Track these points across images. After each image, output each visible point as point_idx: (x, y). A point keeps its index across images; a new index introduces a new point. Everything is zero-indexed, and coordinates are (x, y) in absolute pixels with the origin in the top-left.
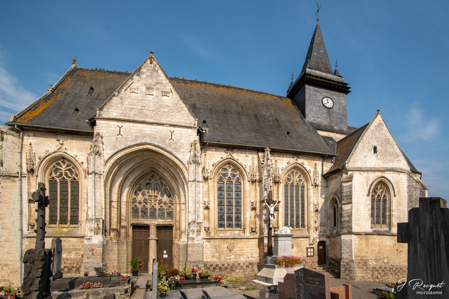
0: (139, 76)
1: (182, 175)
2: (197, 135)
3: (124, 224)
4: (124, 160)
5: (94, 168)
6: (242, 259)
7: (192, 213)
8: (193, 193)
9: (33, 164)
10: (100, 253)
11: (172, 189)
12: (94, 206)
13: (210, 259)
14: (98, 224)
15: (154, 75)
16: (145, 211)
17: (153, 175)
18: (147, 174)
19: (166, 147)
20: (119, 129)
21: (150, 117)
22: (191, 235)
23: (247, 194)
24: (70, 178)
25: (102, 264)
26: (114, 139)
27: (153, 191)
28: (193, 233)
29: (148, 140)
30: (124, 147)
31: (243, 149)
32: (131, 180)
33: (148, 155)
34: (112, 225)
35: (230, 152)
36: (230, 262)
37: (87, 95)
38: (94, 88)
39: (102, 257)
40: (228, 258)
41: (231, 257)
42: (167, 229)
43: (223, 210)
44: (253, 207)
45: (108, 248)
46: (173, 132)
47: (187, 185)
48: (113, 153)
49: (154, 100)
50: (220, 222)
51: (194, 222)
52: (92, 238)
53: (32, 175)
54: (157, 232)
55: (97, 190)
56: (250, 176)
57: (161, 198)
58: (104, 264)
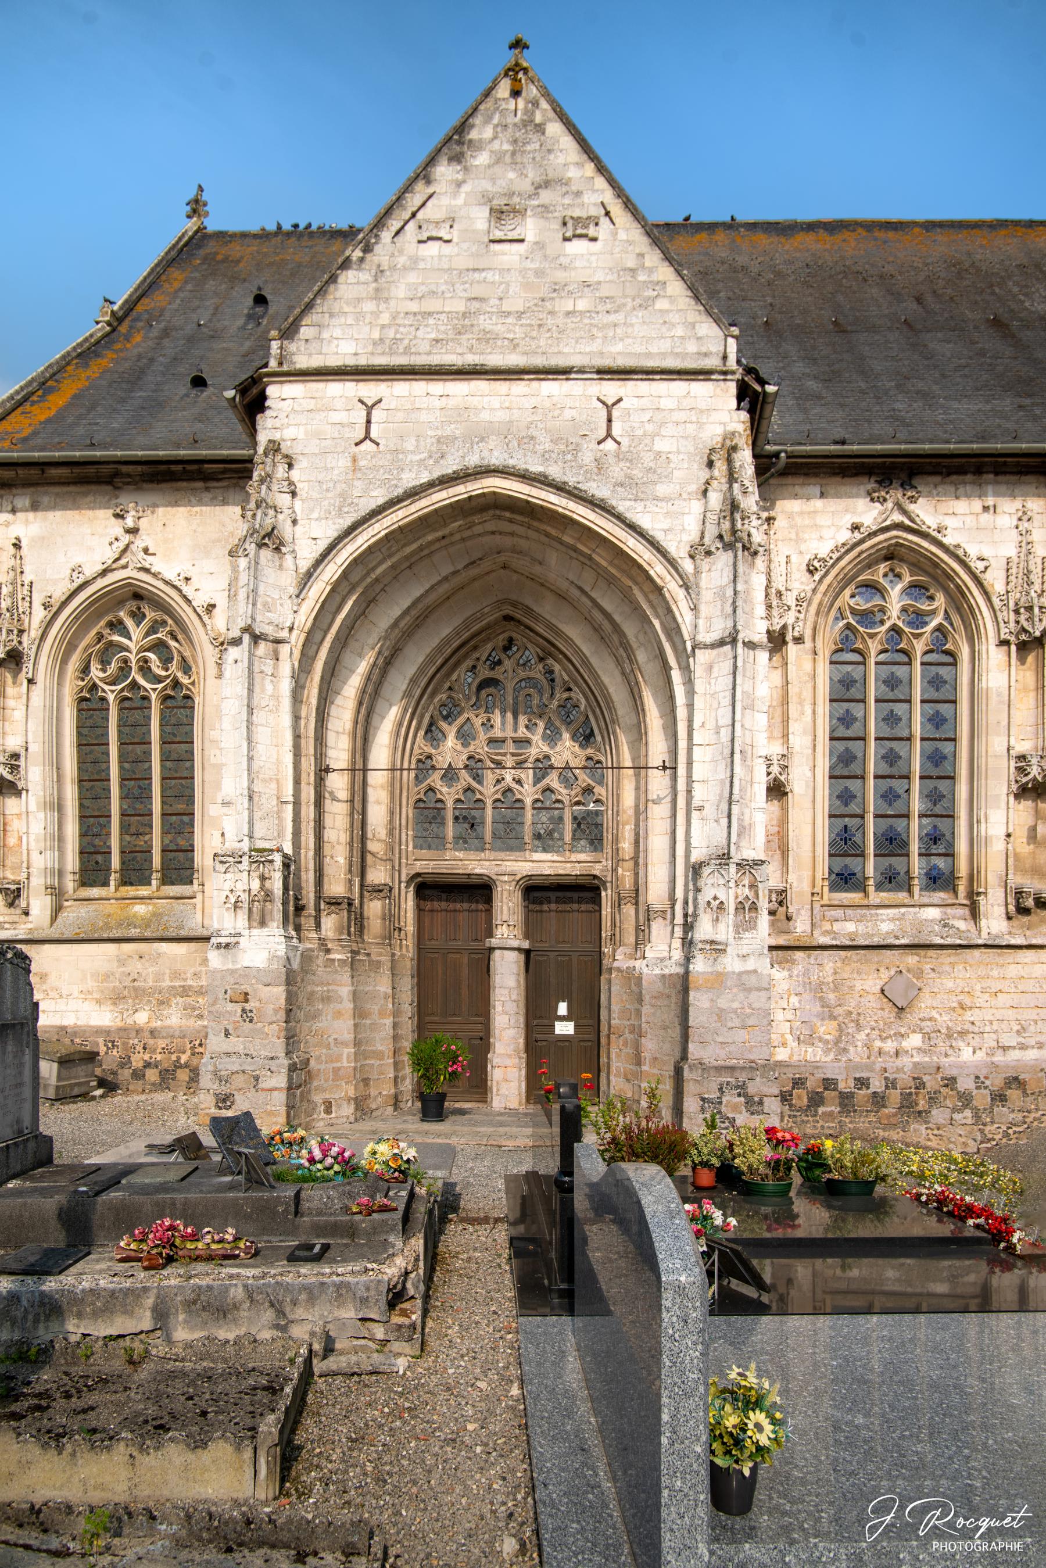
0: (459, 162)
1: (658, 617)
2: (738, 409)
3: (377, 875)
4: (384, 567)
5: (250, 612)
6: (967, 1055)
7: (709, 811)
8: (715, 705)
9: (21, 632)
10: (276, 1011)
11: (600, 702)
12: (246, 792)
13: (788, 1050)
14: (263, 878)
15: (528, 148)
16: (473, 812)
17: (511, 640)
18: (483, 635)
19: (581, 478)
20: (364, 413)
21: (506, 342)
22: (704, 929)
23: (993, 713)
24: (159, 680)
25: (286, 1062)
26: (344, 462)
27: (509, 716)
28: (717, 920)
29: (496, 453)
30: (386, 499)
31: (965, 473)
32: (411, 670)
33: (493, 533)
34: (326, 879)
35: (896, 494)
36: (899, 1070)
37: (243, 328)
38: (269, 297)
39: (287, 1029)
40: (890, 1046)
41: (904, 1044)
42: (571, 901)
43: (859, 800)
44: (1024, 780)
45: (309, 988)
46: (614, 404)
47: (687, 670)
48: (335, 534)
49: (529, 264)
50: (840, 863)
51: (725, 858)
52: (241, 940)
53: (15, 677)
54: (528, 912)
55: (258, 717)
56: (1012, 616)
57: (546, 748)
58: (295, 1064)
